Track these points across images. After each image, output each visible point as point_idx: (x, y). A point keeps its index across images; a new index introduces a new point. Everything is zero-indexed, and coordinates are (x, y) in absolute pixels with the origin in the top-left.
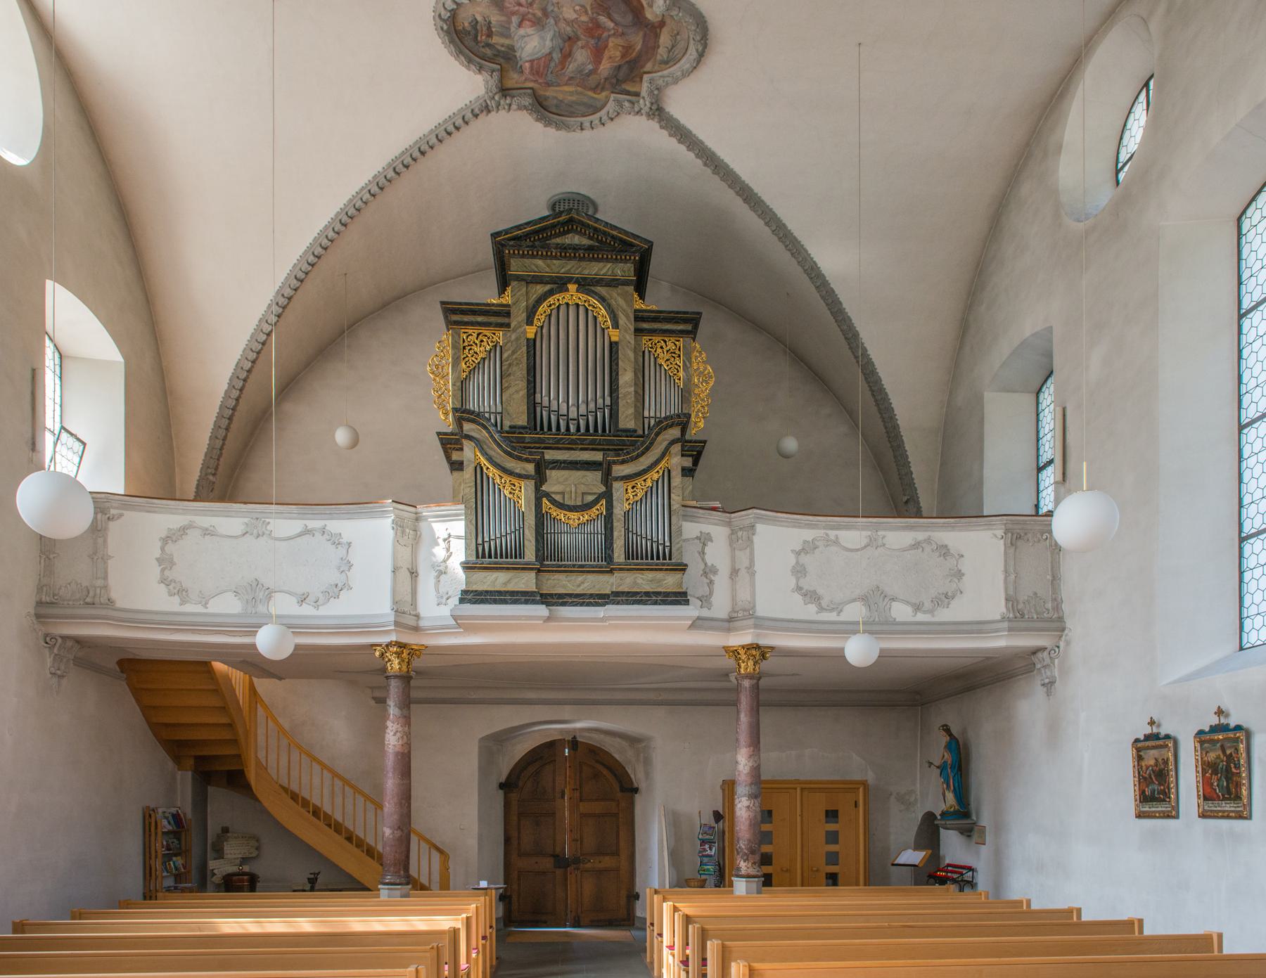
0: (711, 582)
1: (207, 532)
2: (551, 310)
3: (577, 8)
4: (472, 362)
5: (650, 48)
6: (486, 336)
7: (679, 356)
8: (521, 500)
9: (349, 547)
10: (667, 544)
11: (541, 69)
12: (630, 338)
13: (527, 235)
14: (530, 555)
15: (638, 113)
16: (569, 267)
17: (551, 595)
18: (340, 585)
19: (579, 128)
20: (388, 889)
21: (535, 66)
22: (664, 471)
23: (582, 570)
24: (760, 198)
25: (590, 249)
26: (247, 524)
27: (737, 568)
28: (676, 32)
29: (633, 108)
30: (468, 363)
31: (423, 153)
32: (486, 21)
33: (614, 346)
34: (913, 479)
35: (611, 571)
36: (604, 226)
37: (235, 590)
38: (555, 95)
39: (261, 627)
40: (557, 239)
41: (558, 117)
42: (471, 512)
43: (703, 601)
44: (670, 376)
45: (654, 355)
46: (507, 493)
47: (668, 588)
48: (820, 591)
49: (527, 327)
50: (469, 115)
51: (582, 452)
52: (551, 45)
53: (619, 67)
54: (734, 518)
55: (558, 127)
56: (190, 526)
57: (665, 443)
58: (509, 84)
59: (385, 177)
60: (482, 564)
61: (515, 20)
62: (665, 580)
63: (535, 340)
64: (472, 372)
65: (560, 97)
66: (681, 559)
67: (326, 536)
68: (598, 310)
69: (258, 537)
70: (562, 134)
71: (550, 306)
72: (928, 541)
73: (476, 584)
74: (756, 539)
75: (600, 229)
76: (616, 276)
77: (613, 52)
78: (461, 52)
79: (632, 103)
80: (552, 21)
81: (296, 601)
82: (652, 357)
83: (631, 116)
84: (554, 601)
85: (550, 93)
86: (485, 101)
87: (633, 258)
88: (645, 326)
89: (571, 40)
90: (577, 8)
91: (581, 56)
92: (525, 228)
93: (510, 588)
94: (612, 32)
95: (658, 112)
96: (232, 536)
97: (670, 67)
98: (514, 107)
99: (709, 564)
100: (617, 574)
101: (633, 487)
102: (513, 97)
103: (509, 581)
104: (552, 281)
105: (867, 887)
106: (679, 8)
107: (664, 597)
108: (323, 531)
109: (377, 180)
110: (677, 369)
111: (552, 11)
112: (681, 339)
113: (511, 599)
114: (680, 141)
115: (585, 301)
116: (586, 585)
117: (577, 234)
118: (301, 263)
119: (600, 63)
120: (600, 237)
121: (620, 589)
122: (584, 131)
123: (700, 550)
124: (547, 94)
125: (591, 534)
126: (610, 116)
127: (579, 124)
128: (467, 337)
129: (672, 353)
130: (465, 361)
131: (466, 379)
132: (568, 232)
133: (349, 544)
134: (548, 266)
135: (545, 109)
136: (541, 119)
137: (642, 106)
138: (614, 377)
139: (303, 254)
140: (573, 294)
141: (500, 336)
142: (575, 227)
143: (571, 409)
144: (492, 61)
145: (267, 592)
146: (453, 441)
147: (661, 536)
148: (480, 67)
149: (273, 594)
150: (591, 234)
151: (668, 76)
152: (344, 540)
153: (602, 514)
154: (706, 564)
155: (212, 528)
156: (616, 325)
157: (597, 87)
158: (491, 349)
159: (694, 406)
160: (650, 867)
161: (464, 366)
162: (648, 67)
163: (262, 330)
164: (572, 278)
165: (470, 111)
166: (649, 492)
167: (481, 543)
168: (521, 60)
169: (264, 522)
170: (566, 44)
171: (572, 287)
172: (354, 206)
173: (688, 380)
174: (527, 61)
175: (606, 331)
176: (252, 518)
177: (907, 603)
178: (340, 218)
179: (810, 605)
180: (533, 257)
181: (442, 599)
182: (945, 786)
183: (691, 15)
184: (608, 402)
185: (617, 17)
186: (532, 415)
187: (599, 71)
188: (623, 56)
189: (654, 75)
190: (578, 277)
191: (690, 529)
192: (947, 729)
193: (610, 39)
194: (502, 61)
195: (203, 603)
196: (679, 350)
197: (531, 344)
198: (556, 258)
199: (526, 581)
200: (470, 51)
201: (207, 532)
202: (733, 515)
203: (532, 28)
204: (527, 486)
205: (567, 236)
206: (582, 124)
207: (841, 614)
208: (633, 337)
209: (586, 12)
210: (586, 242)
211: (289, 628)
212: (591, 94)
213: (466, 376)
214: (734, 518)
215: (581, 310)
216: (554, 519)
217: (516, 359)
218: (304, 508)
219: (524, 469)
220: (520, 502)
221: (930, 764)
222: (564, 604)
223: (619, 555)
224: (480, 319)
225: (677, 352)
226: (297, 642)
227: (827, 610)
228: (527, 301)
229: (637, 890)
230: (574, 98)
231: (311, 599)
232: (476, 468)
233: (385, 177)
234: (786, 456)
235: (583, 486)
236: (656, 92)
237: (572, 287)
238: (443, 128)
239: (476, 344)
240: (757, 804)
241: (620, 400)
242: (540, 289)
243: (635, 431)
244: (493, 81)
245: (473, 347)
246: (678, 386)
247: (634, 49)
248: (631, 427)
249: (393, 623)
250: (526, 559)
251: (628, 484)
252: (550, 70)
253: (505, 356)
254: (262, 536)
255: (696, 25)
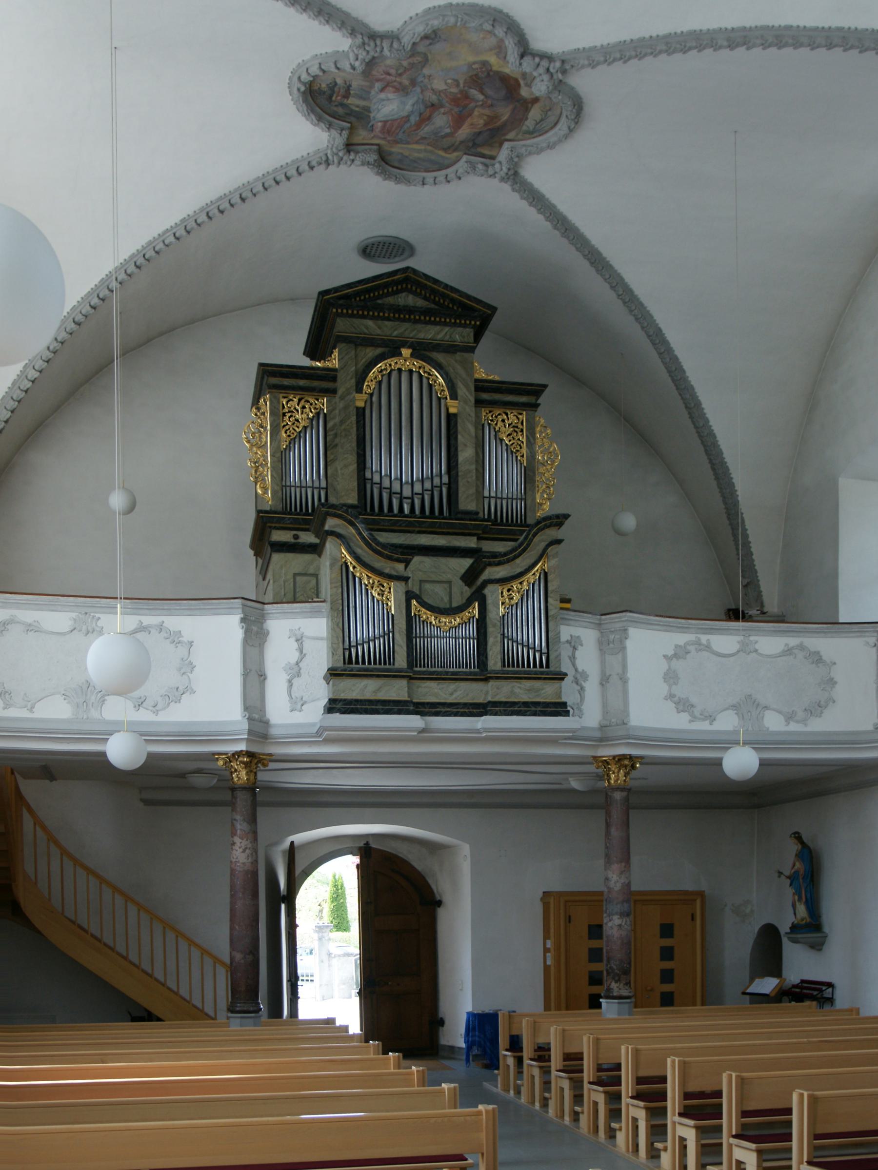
0: (582, 689)
1: (31, 628)
2: (382, 376)
3: (449, 81)
4: (293, 431)
5: (516, 121)
6: (308, 401)
7: (522, 431)
8: (391, 602)
9: (192, 646)
10: (544, 650)
11: (394, 129)
12: (470, 410)
13: (358, 294)
14: (401, 661)
15: (491, 176)
16: (402, 330)
17: (423, 704)
18: (181, 689)
19: (421, 183)
20: (241, 1017)
21: (388, 126)
22: (540, 573)
23: (455, 678)
24: (608, 262)
25: (426, 312)
26: (75, 620)
27: (607, 674)
28: (548, 108)
29: (487, 171)
30: (288, 432)
31: (243, 200)
32: (346, 84)
33: (451, 419)
34: (753, 561)
35: (486, 680)
36: (443, 288)
37: (63, 692)
38: (401, 151)
39: (112, 734)
40: (389, 298)
41: (399, 171)
42: (338, 616)
43: (575, 708)
44: (512, 452)
45: (495, 429)
46: (375, 594)
47: (546, 699)
48: (694, 700)
49: (357, 395)
50: (304, 167)
51: (418, 535)
52: (411, 110)
53: (480, 133)
54: (606, 619)
55: (398, 180)
56: (11, 621)
57: (543, 545)
58: (357, 139)
59: (196, 221)
60: (352, 670)
61: (378, 85)
62: (543, 689)
63: (364, 409)
64: (292, 442)
65: (406, 153)
66: (560, 668)
67: (163, 634)
68: (434, 377)
69: (87, 634)
70: (402, 188)
71: (382, 371)
72: (801, 647)
73: (344, 692)
74: (629, 644)
75: (438, 290)
76: (454, 342)
77: (477, 120)
78: (313, 111)
79: (486, 165)
80: (418, 89)
81: (132, 705)
82: (492, 430)
83: (483, 178)
84: (427, 710)
85: (396, 149)
86: (326, 154)
87: (473, 323)
88: (485, 396)
89: (434, 107)
90: (449, 81)
91: (441, 121)
92: (357, 287)
93: (381, 696)
94: (481, 103)
95: (514, 177)
96: (58, 633)
97: (534, 138)
98: (357, 162)
99: (580, 669)
100: (492, 683)
101: (509, 590)
102: (357, 152)
103: (379, 689)
104: (383, 343)
105: (704, 1007)
106: (560, 91)
107: (543, 707)
108: (160, 627)
109: (185, 224)
110: (520, 445)
111: (422, 82)
112: (524, 413)
113: (382, 709)
114: (531, 204)
115: (420, 368)
116: (459, 693)
117: (411, 294)
118: (82, 306)
119: (460, 128)
120: (437, 299)
121: (496, 699)
122: (425, 186)
123: (571, 655)
124: (393, 150)
125: (466, 638)
126: (458, 174)
127: (421, 179)
128: (287, 403)
129: (514, 427)
130: (284, 429)
131: (285, 449)
132: (398, 292)
133: (191, 643)
134: (380, 328)
135: (387, 163)
136: (382, 173)
137: (498, 170)
138: (452, 453)
139: (85, 296)
140: (406, 360)
141: (324, 403)
142: (409, 286)
143: (405, 487)
144: (342, 119)
145: (99, 695)
146: (275, 520)
147: (538, 638)
148: (330, 125)
149: (106, 698)
150: (428, 295)
151: (532, 146)
152: (185, 639)
153: (473, 617)
154: (576, 670)
155: (36, 624)
156: (454, 396)
157: (449, 148)
158: (313, 416)
159: (538, 487)
160: (461, 990)
161: (284, 435)
162: (511, 135)
163: (26, 377)
164: (407, 342)
165: (307, 163)
166: (525, 596)
167: (348, 647)
168: (374, 120)
169: (93, 617)
170: (428, 110)
171: (406, 352)
172: (154, 248)
173: (532, 457)
174: (381, 121)
175: (443, 401)
176: (80, 613)
177: (780, 712)
178: (135, 259)
179: (682, 714)
180: (363, 317)
181: (297, 704)
182: (796, 898)
183: (570, 97)
184: (445, 479)
185: (489, 92)
186: (363, 493)
187: (456, 135)
188: (485, 125)
189: (516, 143)
190: (412, 342)
191: (566, 632)
192: (798, 837)
193: (476, 109)
194: (353, 119)
195: (29, 707)
196: (522, 424)
197: (361, 413)
198: (388, 319)
199: (397, 690)
200: (322, 109)
201: (31, 628)
202: (603, 617)
203: (396, 94)
204: (397, 587)
205: (400, 295)
206: (424, 178)
207: (714, 723)
208: (473, 409)
209: (458, 85)
210: (420, 303)
211: (141, 735)
212: (441, 153)
213: (287, 446)
214: (606, 619)
215: (415, 377)
216: (423, 622)
217: (345, 430)
218: (141, 603)
219: (394, 569)
220: (389, 604)
221: (780, 873)
222: (437, 714)
223: (494, 662)
224: (302, 383)
225: (520, 426)
226: (148, 750)
227: (700, 719)
228: (356, 365)
229: (441, 1015)
230: (421, 155)
231: (149, 703)
232: (342, 566)
233: (196, 221)
234: (619, 533)
235: (421, 573)
236: (516, 160)
237: (406, 352)
238: (272, 176)
239: (297, 411)
240: (628, 923)
241: (460, 479)
242: (371, 353)
243: (477, 513)
244: (340, 140)
245: (294, 414)
246: (521, 464)
247: (500, 120)
248: (472, 509)
249: (246, 731)
250: (397, 665)
251: (504, 586)
252: (402, 130)
253: (330, 425)
254: (92, 632)
255: (573, 107)
